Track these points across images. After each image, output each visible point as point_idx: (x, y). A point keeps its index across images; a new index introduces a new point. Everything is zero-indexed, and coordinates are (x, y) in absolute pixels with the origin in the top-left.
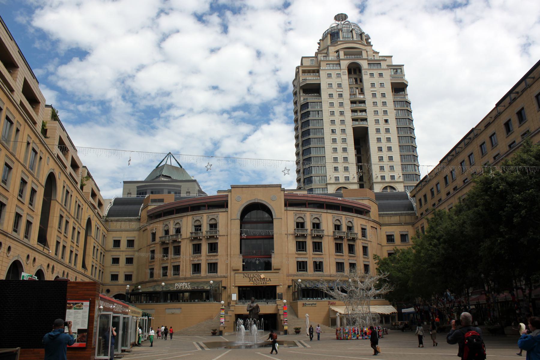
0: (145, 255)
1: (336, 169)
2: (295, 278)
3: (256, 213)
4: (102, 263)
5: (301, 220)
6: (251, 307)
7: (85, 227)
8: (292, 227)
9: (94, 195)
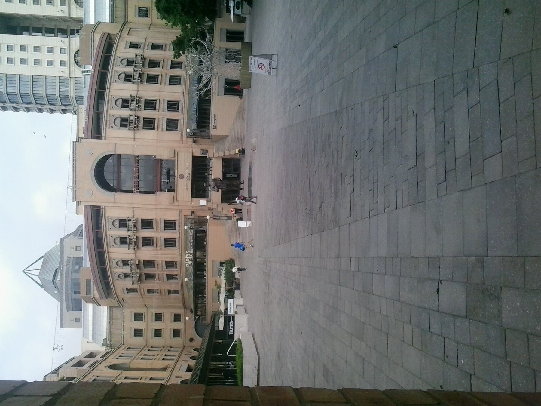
0: (154, 299)
1: (50, 63)
2: (185, 135)
3: (106, 173)
4: (160, 349)
5: (118, 122)
6: (214, 187)
7: (119, 371)
8: (125, 133)
9: (80, 364)
